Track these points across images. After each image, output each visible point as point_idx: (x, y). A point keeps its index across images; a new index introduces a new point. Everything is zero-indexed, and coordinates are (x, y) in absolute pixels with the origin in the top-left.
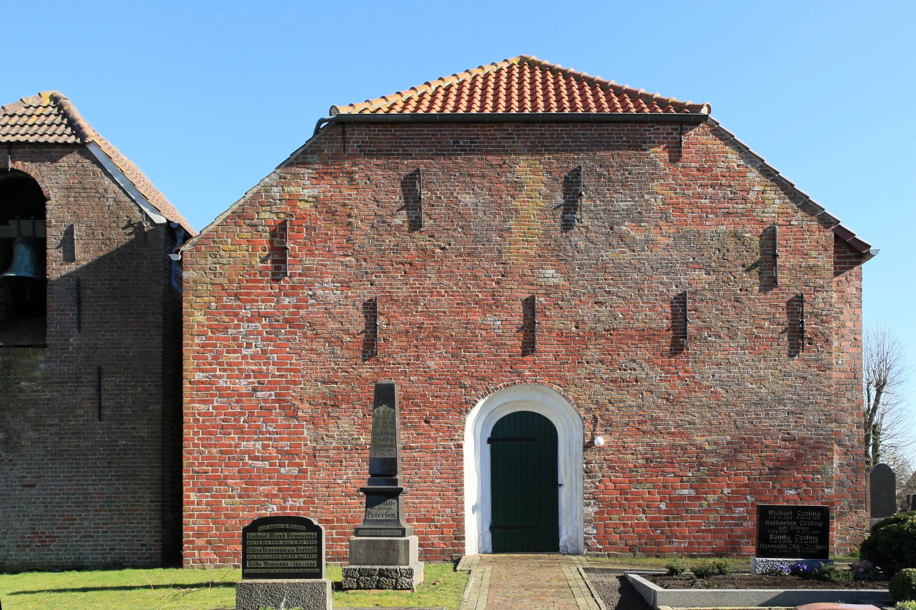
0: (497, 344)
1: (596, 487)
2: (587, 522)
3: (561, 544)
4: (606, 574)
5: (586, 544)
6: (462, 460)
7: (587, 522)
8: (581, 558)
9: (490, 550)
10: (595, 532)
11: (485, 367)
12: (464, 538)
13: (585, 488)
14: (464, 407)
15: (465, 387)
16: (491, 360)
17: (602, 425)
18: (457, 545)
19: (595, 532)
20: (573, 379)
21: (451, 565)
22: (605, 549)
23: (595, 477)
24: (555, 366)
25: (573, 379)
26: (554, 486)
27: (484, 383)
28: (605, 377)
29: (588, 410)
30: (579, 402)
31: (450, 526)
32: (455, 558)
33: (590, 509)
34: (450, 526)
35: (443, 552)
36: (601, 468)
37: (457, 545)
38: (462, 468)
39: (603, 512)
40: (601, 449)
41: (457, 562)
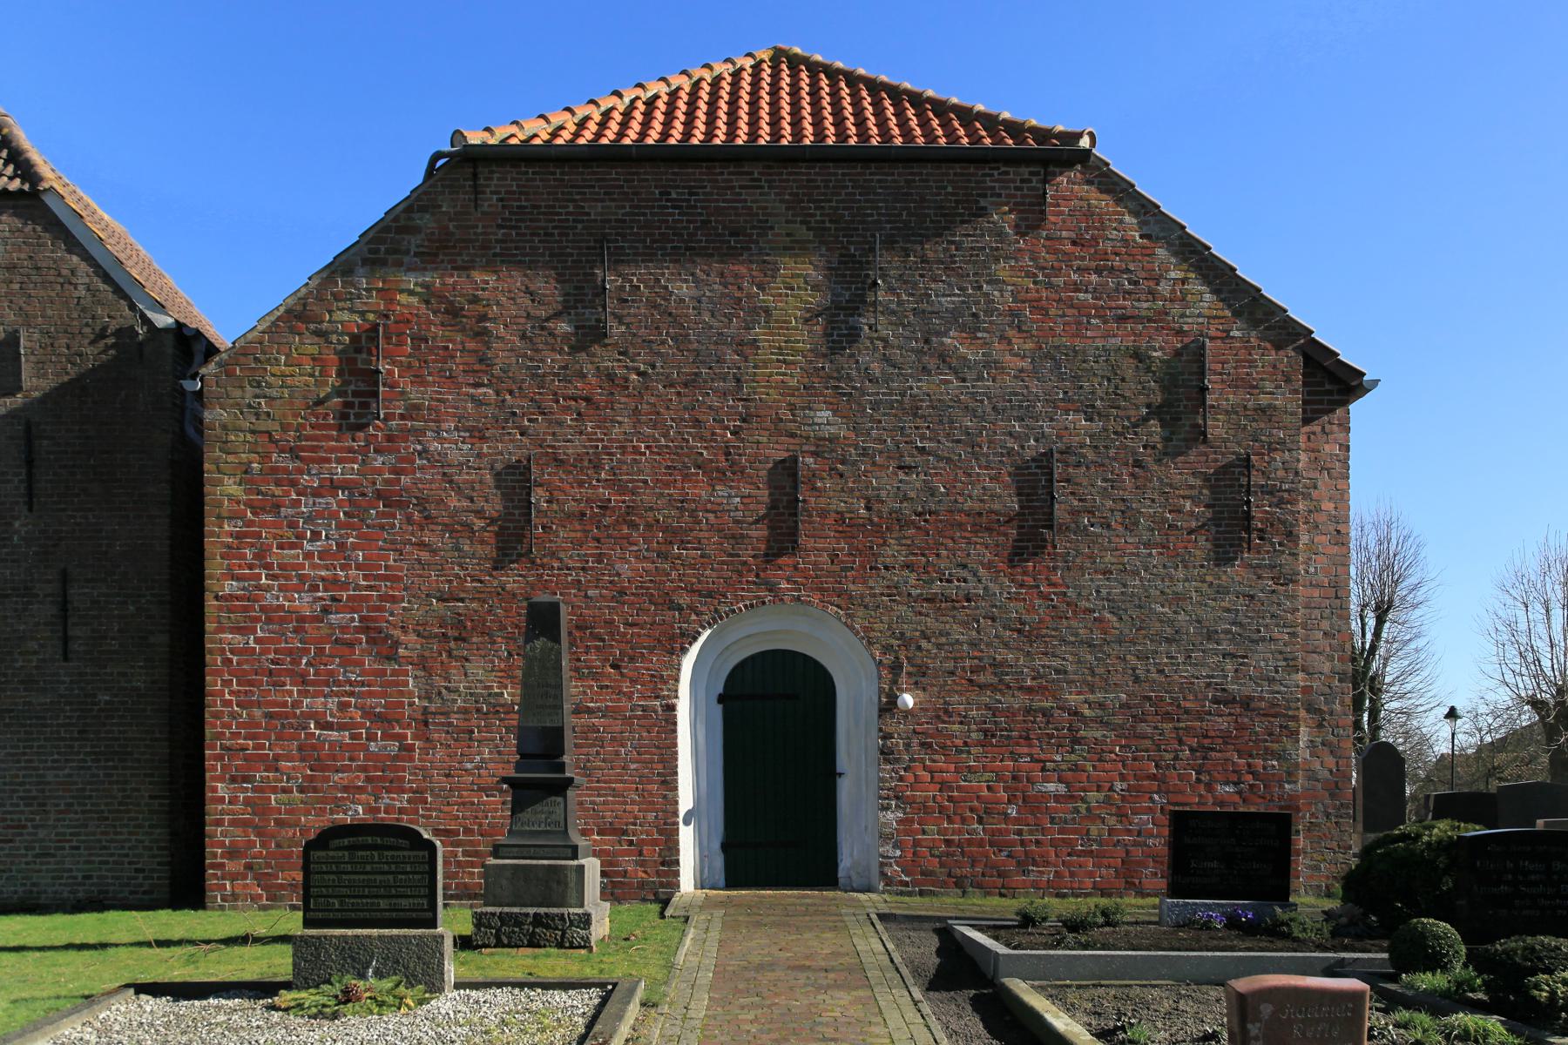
0: (733, 536)
1: (901, 779)
2: (885, 838)
3: (840, 874)
4: (916, 925)
5: (883, 874)
6: (675, 731)
7: (885, 838)
8: (873, 896)
9: (722, 882)
10: (898, 853)
11: (714, 574)
12: (677, 863)
13: (882, 780)
14: (676, 645)
15: (680, 609)
16: (723, 563)
17: (909, 674)
18: (666, 874)
19: (898, 853)
20: (862, 597)
21: (656, 907)
22: (915, 883)
23: (897, 760)
24: (830, 573)
25: (862, 597)
26: (830, 775)
27: (711, 603)
28: (915, 592)
29: (887, 649)
30: (872, 634)
31: (655, 843)
32: (662, 897)
33: (890, 815)
34: (655, 843)
35: (642, 885)
36: (908, 745)
37: (666, 874)
38: (675, 745)
39: (912, 821)
40: (907, 713)
41: (665, 903)
